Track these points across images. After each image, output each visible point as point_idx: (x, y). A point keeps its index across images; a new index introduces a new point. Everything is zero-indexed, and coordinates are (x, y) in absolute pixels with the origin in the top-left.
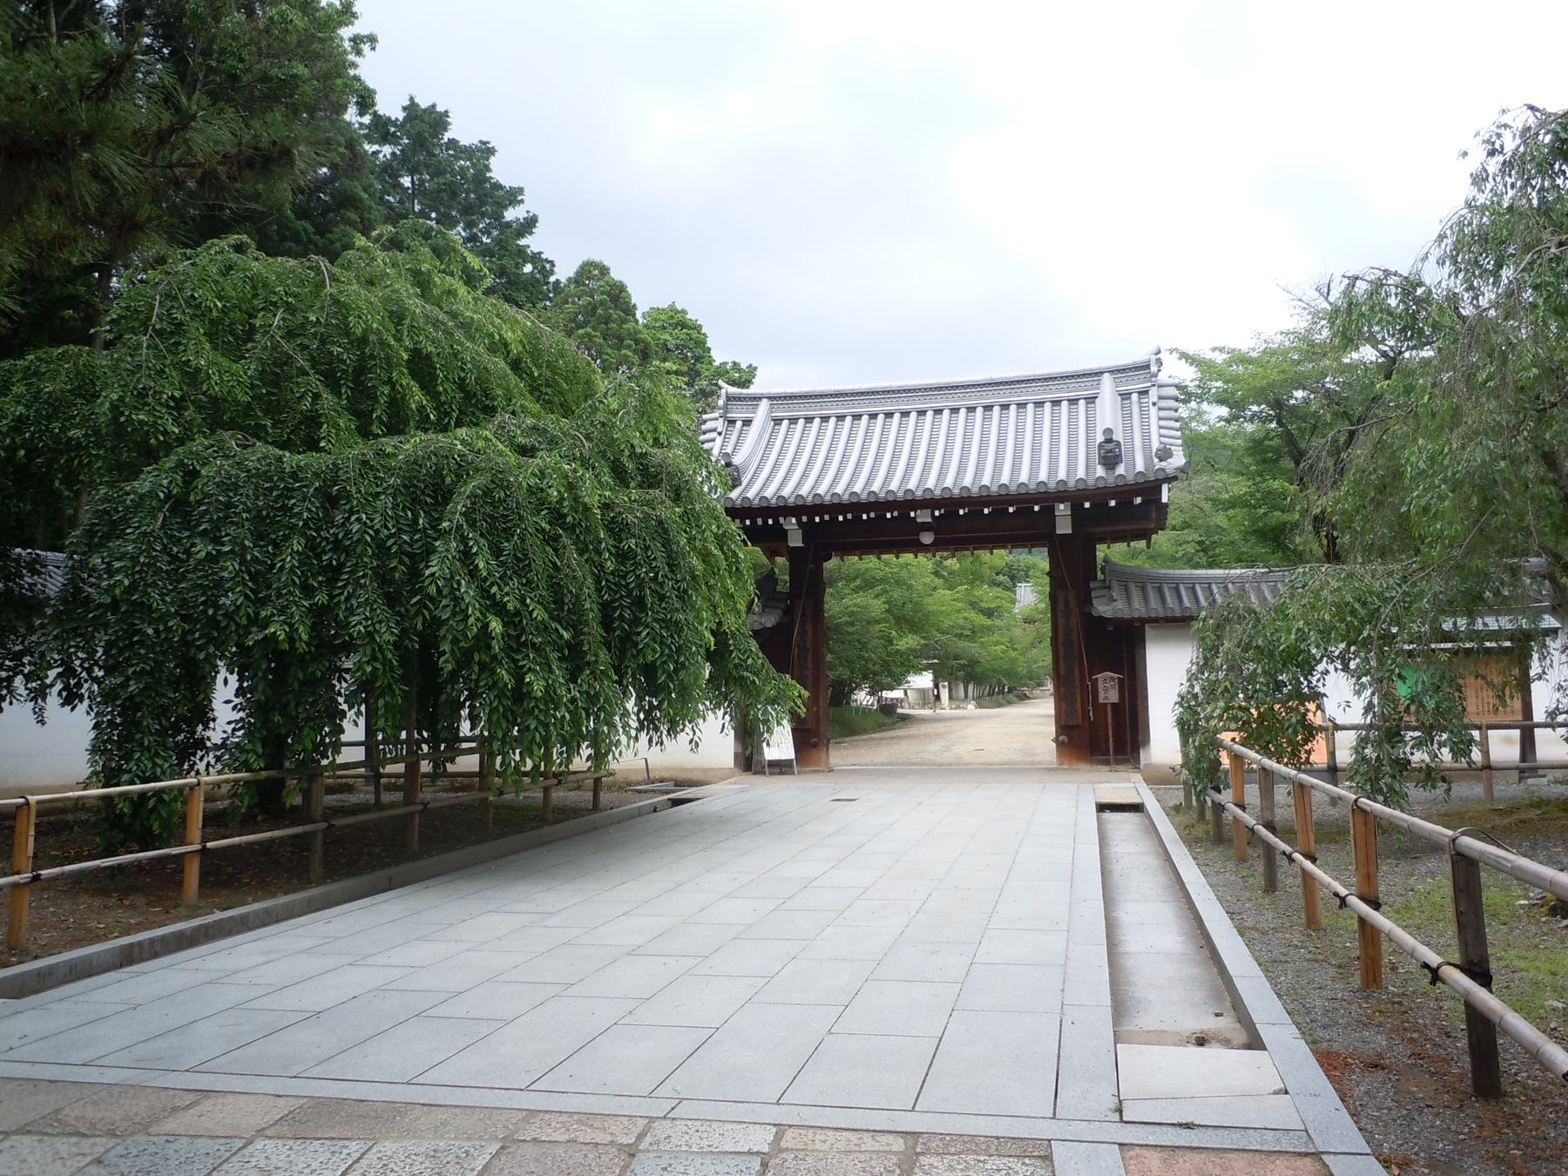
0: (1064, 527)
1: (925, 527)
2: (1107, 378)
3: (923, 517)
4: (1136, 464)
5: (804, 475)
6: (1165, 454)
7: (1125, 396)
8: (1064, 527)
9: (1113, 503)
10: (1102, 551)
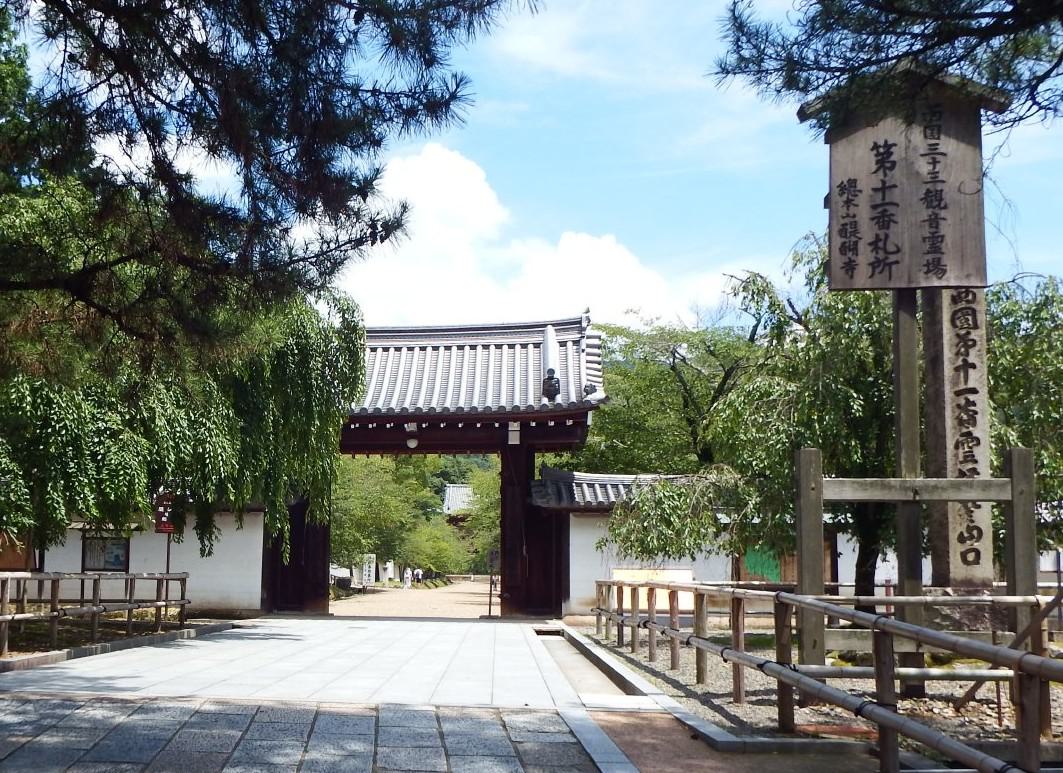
0: (514, 439)
1: (411, 435)
2: (550, 330)
3: (410, 427)
4: (568, 395)
5: (418, 391)
6: (591, 390)
7: (563, 344)
8: (514, 439)
9: (534, 424)
10: (538, 460)
